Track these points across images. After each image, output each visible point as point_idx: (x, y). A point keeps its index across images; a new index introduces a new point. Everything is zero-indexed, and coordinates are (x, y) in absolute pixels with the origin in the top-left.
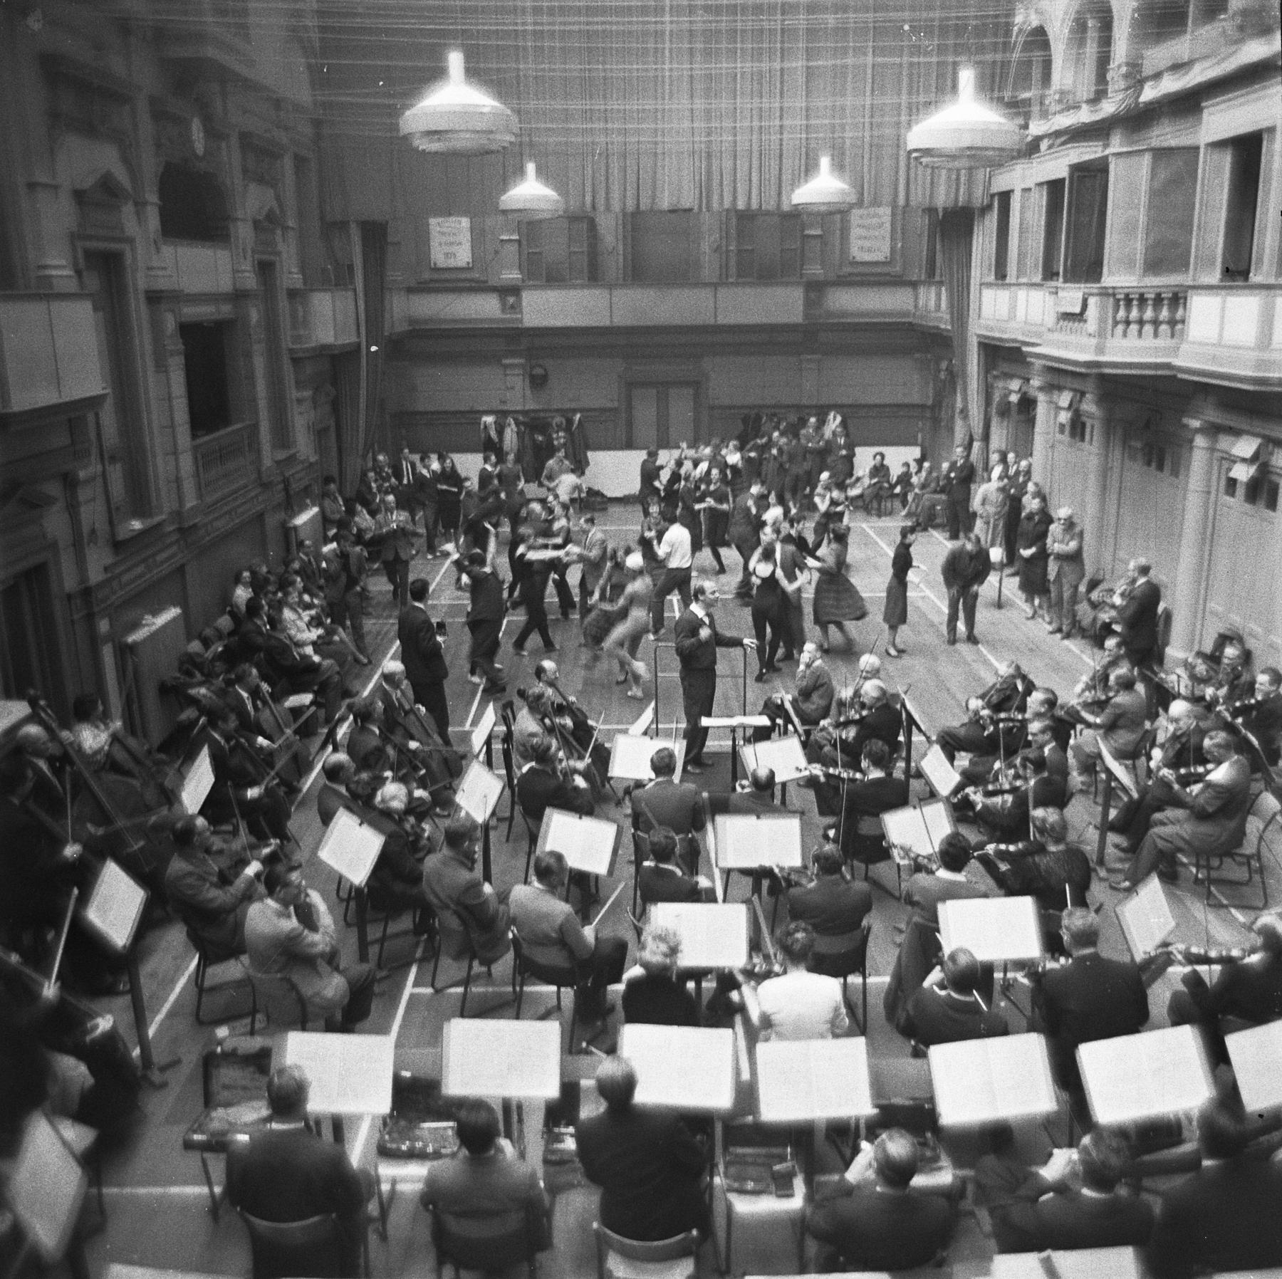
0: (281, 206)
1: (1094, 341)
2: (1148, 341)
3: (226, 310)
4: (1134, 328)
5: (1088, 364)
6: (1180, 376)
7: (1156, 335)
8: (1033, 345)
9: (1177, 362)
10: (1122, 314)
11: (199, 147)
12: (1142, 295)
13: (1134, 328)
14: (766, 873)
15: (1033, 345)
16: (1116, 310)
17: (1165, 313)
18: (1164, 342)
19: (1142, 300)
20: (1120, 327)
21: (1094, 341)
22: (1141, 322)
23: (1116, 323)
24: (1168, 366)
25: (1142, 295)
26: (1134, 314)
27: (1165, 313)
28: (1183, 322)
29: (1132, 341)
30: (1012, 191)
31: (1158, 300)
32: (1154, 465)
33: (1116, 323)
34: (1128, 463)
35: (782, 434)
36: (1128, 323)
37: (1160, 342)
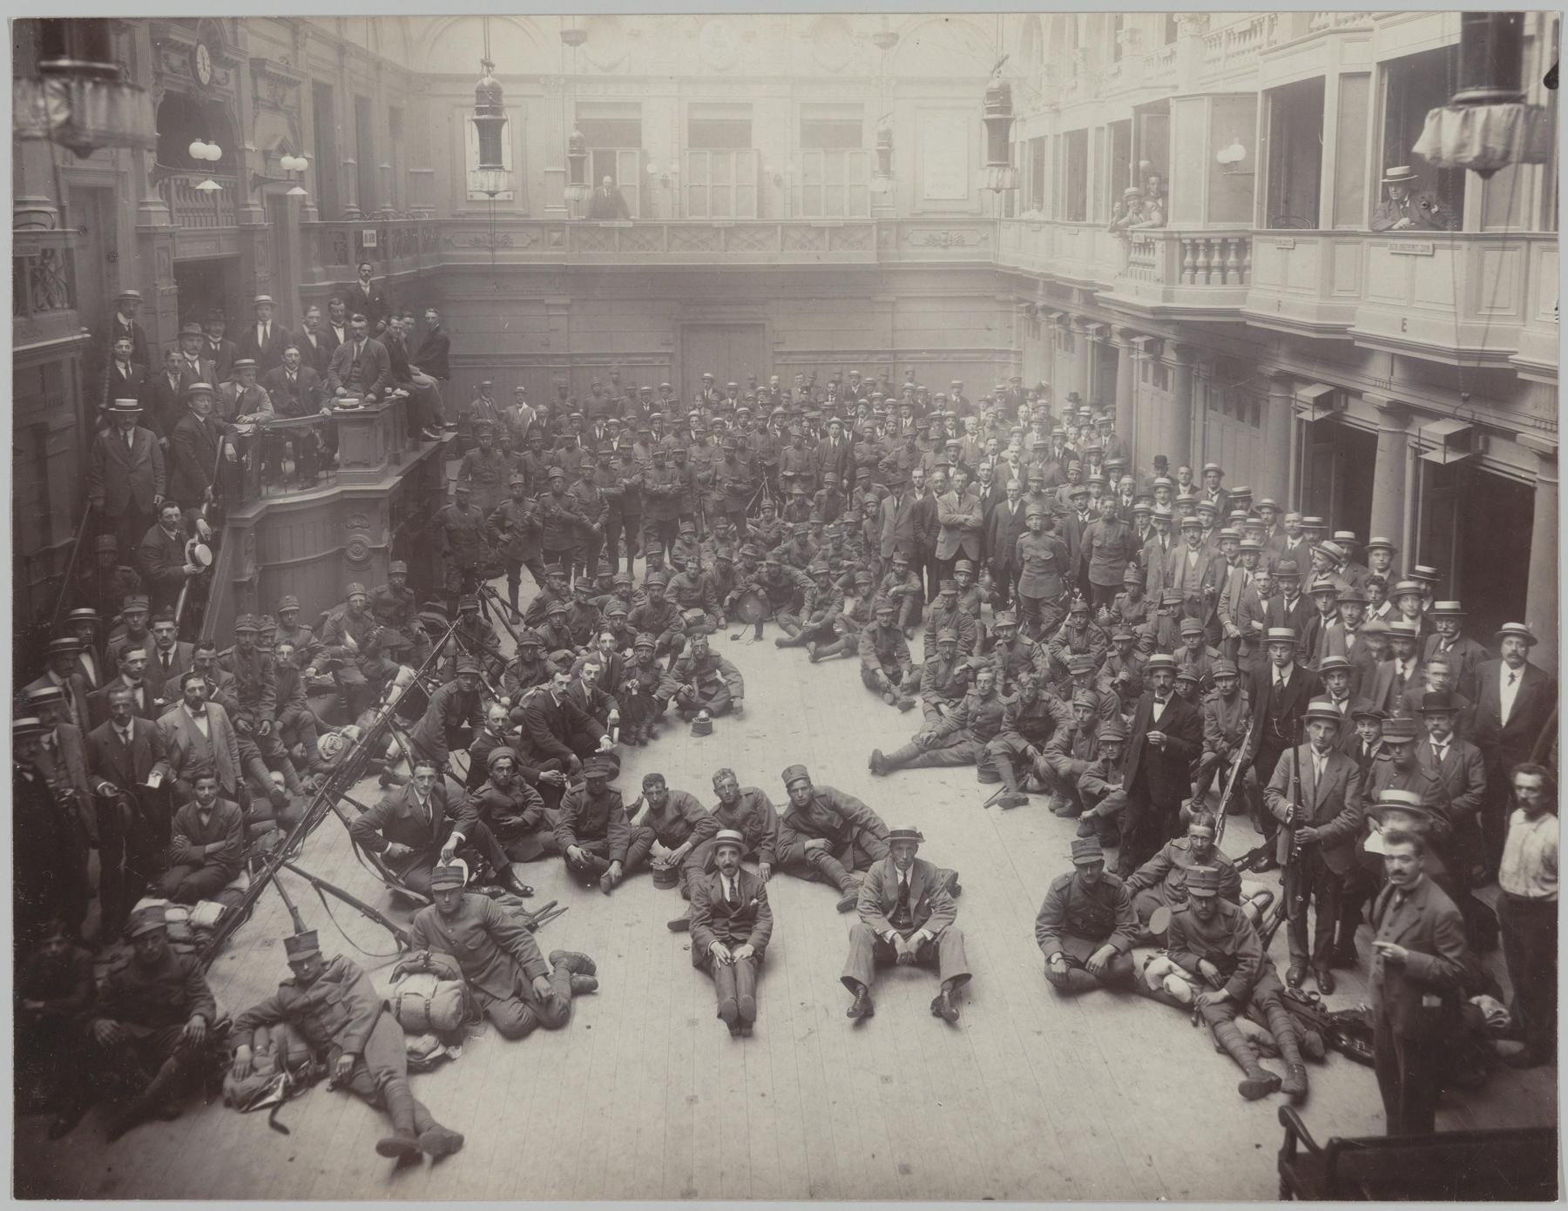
0: (294, 132)
1: (1161, 287)
2: (1216, 288)
3: (227, 250)
4: (1201, 274)
5: (1154, 311)
6: (1249, 323)
7: (1208, 281)
8: (1110, 289)
9: (1245, 308)
10: (1188, 259)
11: (205, 77)
12: (1208, 240)
13: (1201, 274)
14: (1040, 944)
15: (1110, 289)
16: (1183, 254)
17: (1232, 259)
18: (1232, 288)
19: (1209, 246)
20: (1188, 272)
21: (1161, 287)
22: (1208, 268)
23: (1183, 269)
24: (1236, 313)
25: (1225, 240)
26: (1201, 259)
27: (1232, 259)
28: (1250, 267)
29: (1200, 288)
30: (1322, 78)
31: (1195, 247)
32: (1248, 416)
33: (1183, 269)
34: (1210, 413)
35: (401, 317)
36: (1195, 269)
37: (1210, 289)
